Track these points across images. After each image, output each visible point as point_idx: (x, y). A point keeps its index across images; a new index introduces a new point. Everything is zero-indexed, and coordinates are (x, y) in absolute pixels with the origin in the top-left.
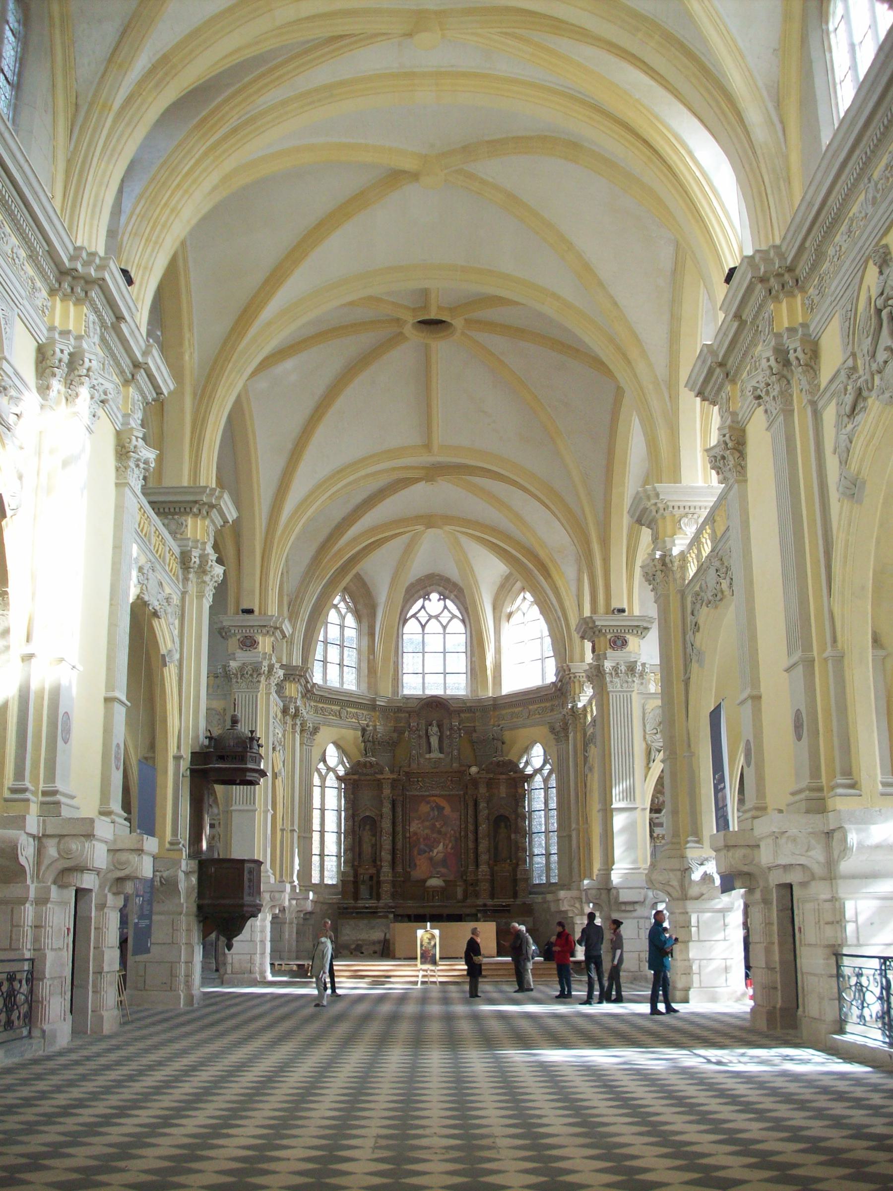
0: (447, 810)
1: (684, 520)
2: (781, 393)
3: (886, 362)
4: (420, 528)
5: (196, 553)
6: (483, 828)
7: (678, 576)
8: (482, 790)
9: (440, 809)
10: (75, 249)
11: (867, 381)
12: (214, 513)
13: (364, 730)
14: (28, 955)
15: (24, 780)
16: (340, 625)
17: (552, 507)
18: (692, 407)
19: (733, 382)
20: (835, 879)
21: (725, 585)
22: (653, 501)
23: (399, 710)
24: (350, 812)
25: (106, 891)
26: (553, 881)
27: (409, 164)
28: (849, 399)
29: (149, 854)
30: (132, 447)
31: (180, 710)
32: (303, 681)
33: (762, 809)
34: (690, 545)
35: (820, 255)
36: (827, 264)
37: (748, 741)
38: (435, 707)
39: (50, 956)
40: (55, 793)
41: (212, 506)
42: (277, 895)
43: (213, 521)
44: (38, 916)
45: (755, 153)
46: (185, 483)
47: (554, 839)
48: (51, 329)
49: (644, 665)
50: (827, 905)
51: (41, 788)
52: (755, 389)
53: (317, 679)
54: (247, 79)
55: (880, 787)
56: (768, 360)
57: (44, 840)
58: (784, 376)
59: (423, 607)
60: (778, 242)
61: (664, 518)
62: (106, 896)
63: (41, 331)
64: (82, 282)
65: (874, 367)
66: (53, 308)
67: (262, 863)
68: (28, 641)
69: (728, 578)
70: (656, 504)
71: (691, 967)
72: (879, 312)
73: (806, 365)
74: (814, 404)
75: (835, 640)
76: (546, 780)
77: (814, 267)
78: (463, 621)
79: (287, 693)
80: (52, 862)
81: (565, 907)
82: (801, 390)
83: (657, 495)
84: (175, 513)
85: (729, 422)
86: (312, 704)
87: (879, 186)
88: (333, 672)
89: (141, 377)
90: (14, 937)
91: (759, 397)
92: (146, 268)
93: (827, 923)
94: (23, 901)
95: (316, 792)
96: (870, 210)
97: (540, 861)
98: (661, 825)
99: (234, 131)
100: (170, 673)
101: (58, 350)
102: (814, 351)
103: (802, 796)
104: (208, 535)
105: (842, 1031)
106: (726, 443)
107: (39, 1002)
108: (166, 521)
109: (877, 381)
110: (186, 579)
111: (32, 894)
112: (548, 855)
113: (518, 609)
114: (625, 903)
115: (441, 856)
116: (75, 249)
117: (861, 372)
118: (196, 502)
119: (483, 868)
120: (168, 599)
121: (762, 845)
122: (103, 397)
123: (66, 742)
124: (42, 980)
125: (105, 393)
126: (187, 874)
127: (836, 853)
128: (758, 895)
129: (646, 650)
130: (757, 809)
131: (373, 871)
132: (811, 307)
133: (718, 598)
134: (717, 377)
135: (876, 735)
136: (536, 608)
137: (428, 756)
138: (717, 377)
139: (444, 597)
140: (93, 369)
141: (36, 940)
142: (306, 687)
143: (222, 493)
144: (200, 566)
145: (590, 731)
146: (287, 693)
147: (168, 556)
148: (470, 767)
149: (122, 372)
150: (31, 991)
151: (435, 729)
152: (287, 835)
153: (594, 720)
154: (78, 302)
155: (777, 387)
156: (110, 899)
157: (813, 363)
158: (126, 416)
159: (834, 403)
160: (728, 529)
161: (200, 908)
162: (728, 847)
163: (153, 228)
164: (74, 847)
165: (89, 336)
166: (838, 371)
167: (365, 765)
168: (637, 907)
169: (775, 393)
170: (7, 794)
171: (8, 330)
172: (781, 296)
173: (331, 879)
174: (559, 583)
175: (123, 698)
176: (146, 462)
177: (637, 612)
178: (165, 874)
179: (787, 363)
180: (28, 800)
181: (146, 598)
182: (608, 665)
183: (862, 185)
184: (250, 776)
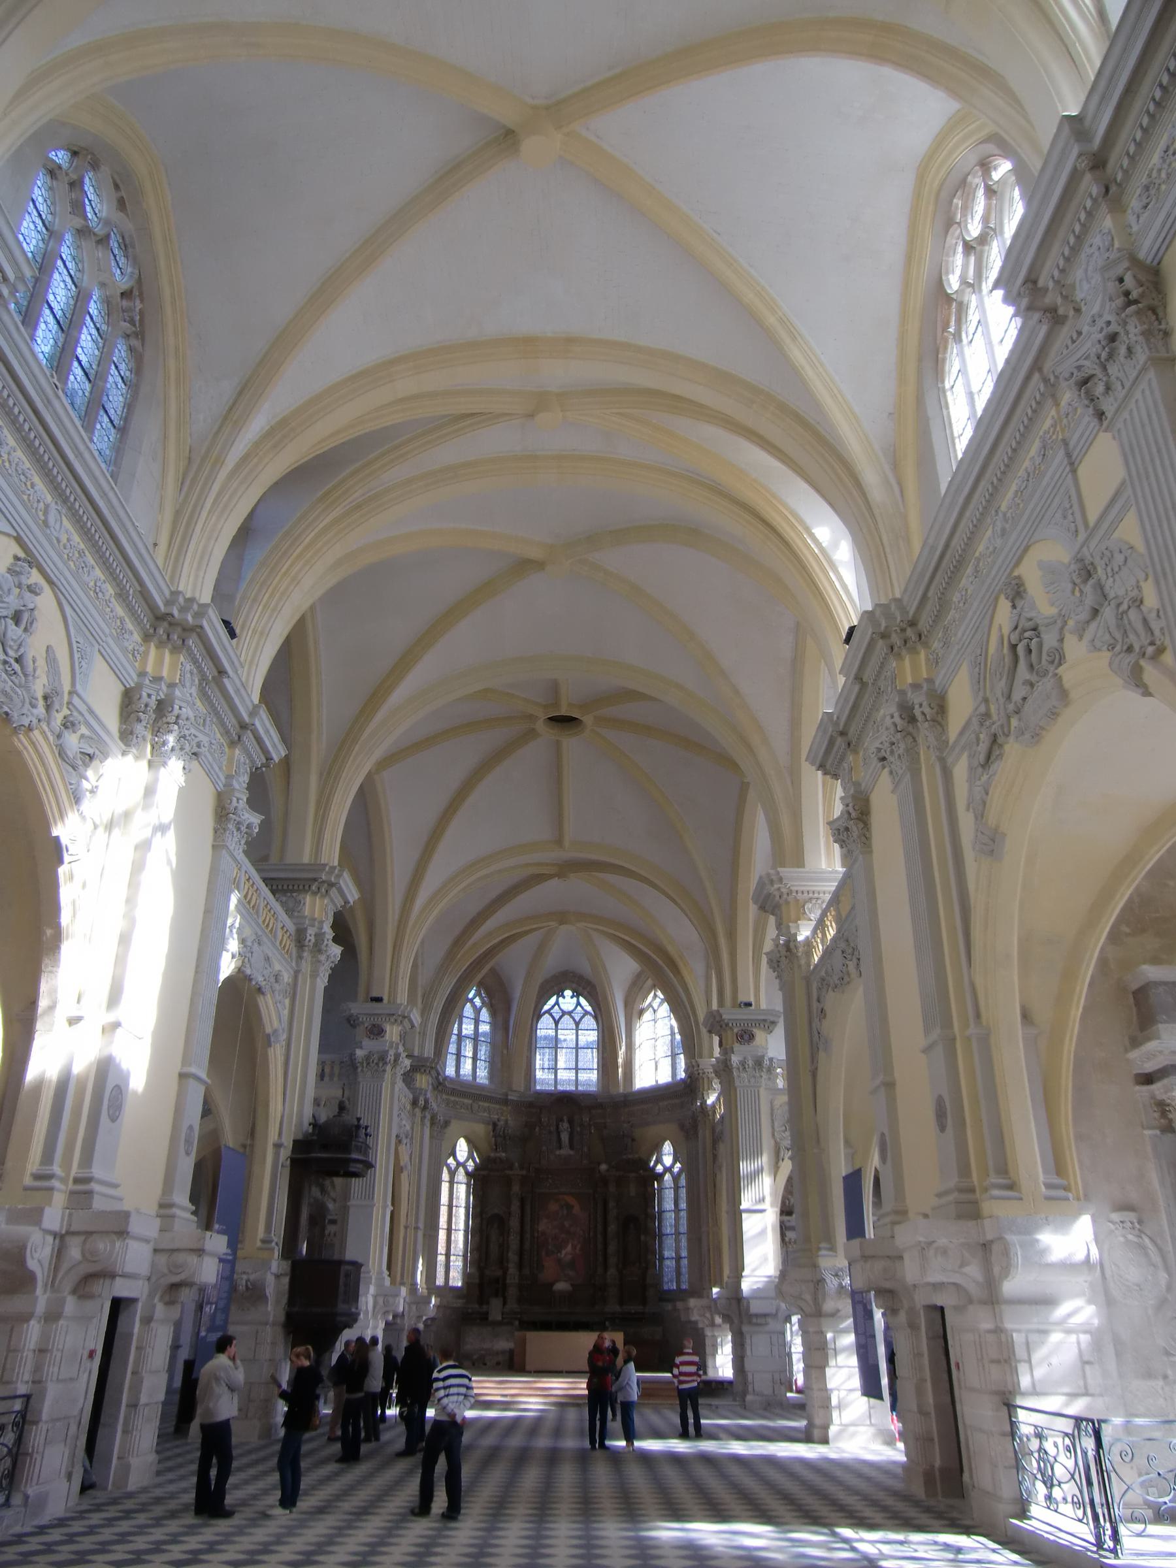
0: (577, 1209)
1: (808, 906)
2: (907, 750)
3: (1024, 699)
4: (553, 924)
5: (311, 932)
6: (612, 1228)
7: (803, 962)
8: (612, 1188)
9: (569, 1207)
10: (172, 593)
11: (1002, 726)
12: (334, 892)
13: (495, 1125)
14: (22, 1389)
15: (52, 1164)
16: (474, 1021)
17: (679, 901)
18: (814, 781)
19: (856, 752)
20: (998, 1303)
21: (851, 966)
22: (776, 886)
23: (531, 1105)
24: (478, 1210)
25: (156, 1300)
26: (684, 1287)
27: (535, 553)
28: (983, 748)
29: (212, 1254)
30: (232, 808)
31: (284, 1094)
32: (434, 1073)
33: (901, 1214)
34: (814, 932)
35: (944, 604)
36: (952, 612)
37: (883, 1134)
38: (566, 1103)
39: (52, 1391)
40: (88, 1180)
41: (331, 885)
42: (391, 1300)
43: (332, 901)
44: (45, 1336)
45: (873, 515)
46: (306, 860)
47: (684, 1242)
48: (142, 674)
49: (771, 1060)
50: (991, 1338)
51: (73, 1173)
52: (879, 750)
53: (450, 1071)
54: (372, 456)
55: (1043, 1188)
56: (892, 717)
57: (68, 1238)
58: (909, 734)
59: (557, 1003)
60: (898, 595)
61: (787, 903)
62: (154, 1306)
63: (129, 674)
64: (179, 629)
65: (1011, 707)
66: (146, 654)
67: (361, 1265)
68: (79, 1001)
69: (855, 960)
70: (779, 889)
71: (829, 1399)
72: (1014, 647)
73: (933, 720)
74: (942, 760)
75: (978, 1016)
76: (676, 1178)
77: (937, 618)
78: (596, 1018)
79: (418, 1085)
80: (74, 1266)
81: (695, 1317)
82: (928, 747)
83: (781, 880)
84: (292, 891)
85: (852, 791)
86: (444, 1096)
87: (1009, 515)
88: (467, 1067)
89: (248, 738)
90: (8, 1366)
91: (884, 759)
92: (262, 634)
93: (993, 1361)
94: (26, 1318)
95: (445, 1187)
96: (999, 542)
97: (670, 1264)
98: (792, 1228)
99: (358, 507)
100: (276, 1054)
101: (144, 694)
102: (940, 706)
103: (950, 1198)
104: (326, 913)
105: (1023, 1514)
106: (849, 814)
107: (27, 1454)
108: (284, 899)
109: (1014, 722)
110: (300, 957)
111: (41, 1307)
112: (678, 1259)
113: (650, 1005)
114: (757, 1316)
115: (569, 1257)
116: (172, 593)
117: (995, 717)
118: (315, 880)
119: (612, 1271)
120: (277, 977)
121: (906, 1256)
122: (195, 749)
123: (114, 1119)
124: (36, 1423)
125: (199, 746)
126: (277, 1276)
127: (996, 1270)
128: (902, 1317)
129: (774, 1045)
130: (897, 1212)
131: (499, 1273)
132: (935, 662)
133: (843, 982)
134: (838, 747)
135: (1033, 1124)
136: (666, 1006)
137: (558, 1152)
138: (838, 747)
139: (577, 994)
140: (184, 717)
141: (38, 1369)
142: (437, 1078)
143: (341, 871)
144: (316, 944)
145: (718, 1129)
146: (418, 1085)
147: (280, 933)
148: (599, 1164)
149: (227, 732)
150: (19, 1440)
151: (566, 1125)
152: (411, 1232)
153: (722, 1117)
154: (175, 650)
155: (902, 746)
156: (160, 1310)
157: (939, 718)
158: (229, 777)
159: (965, 757)
160: (853, 908)
161: (289, 1316)
162: (865, 1258)
163: (272, 596)
164: (101, 1246)
165: (184, 686)
166: (970, 719)
167: (494, 1160)
168: (769, 1320)
169: (901, 751)
170: (28, 1181)
171: (83, 663)
172: (904, 652)
173: (456, 1280)
174: (688, 979)
175: (204, 1076)
176: (249, 826)
177: (763, 1006)
178: (252, 1277)
179: (912, 720)
180: (51, 1189)
181: (248, 972)
182: (735, 1059)
183: (989, 520)
184: (353, 1168)
